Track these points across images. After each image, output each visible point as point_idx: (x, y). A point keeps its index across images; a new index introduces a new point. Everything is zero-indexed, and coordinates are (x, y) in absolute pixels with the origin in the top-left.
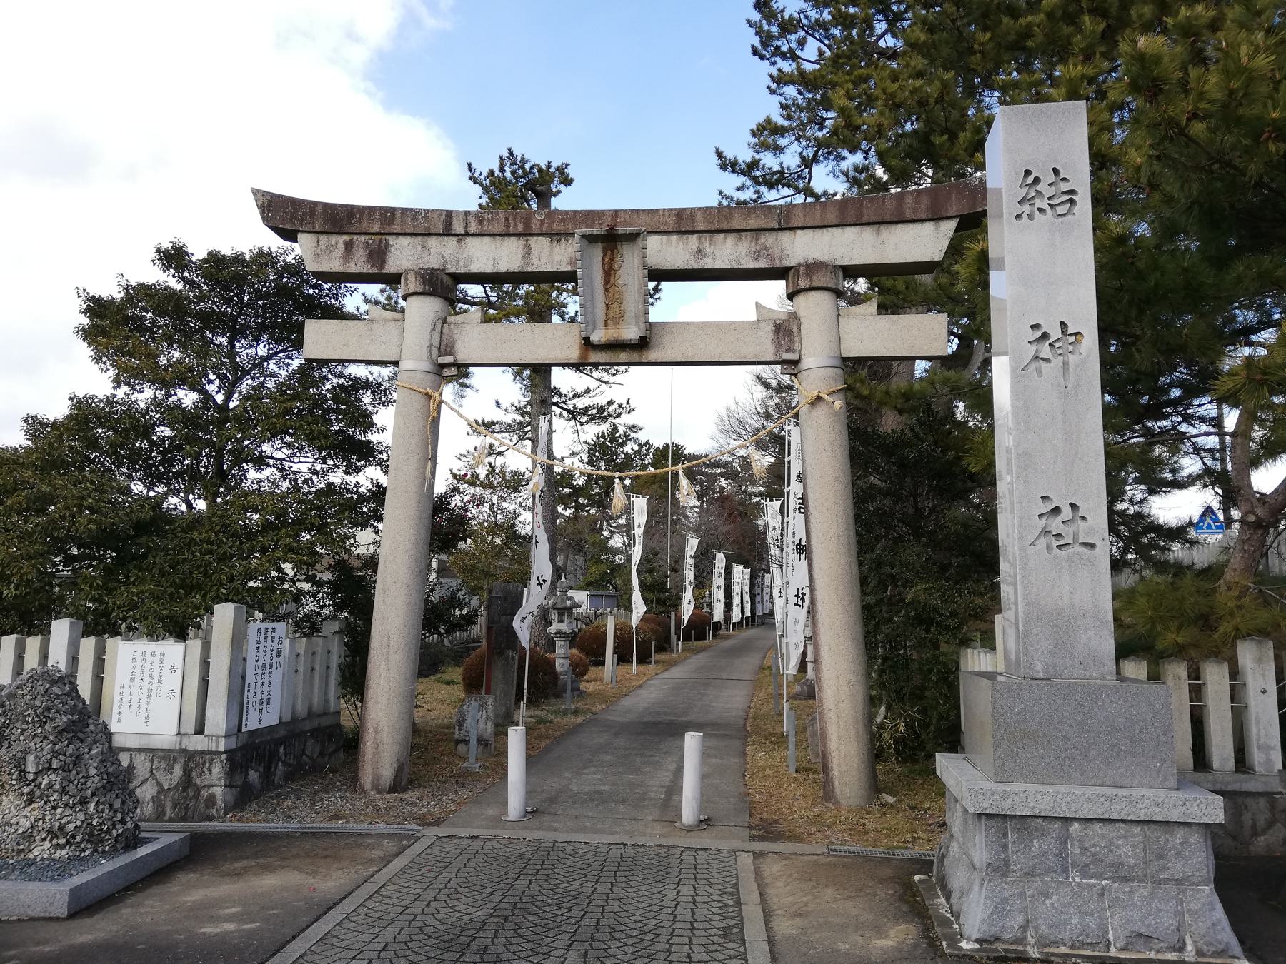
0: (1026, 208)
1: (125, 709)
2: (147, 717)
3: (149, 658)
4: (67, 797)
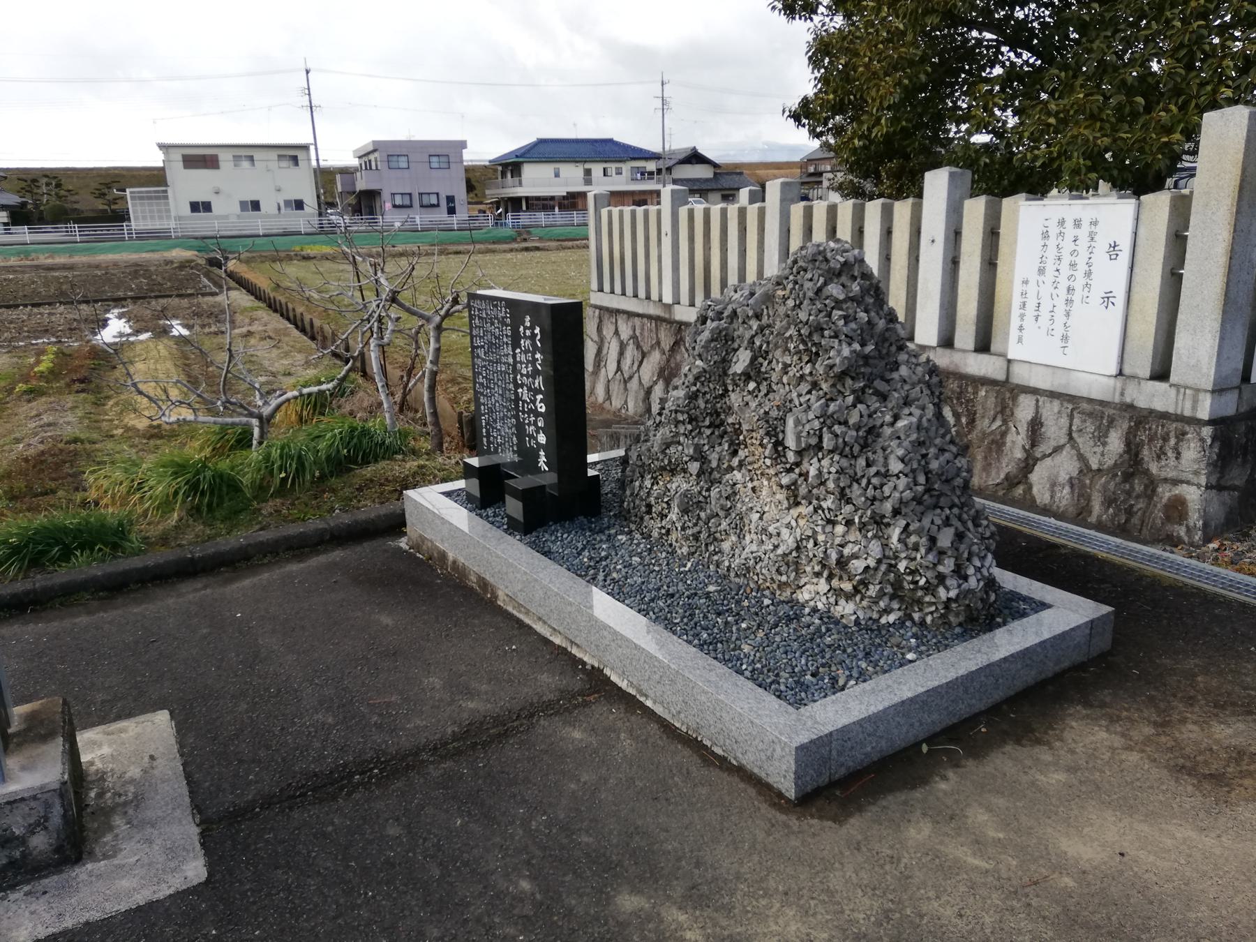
1: (1029, 322)
2: (1065, 338)
3: (1070, 231)
4: (849, 508)
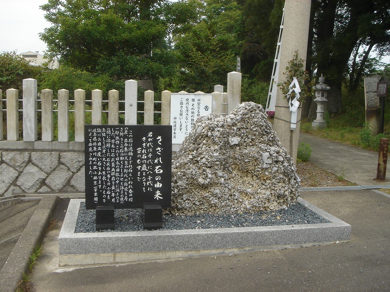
3: (191, 102)
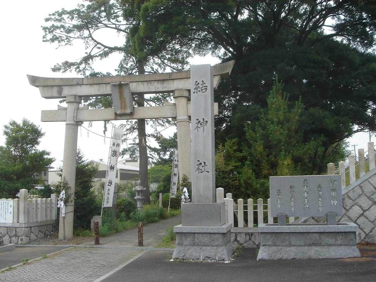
0: (196, 91)
2: (5, 219)
3: (5, 204)
